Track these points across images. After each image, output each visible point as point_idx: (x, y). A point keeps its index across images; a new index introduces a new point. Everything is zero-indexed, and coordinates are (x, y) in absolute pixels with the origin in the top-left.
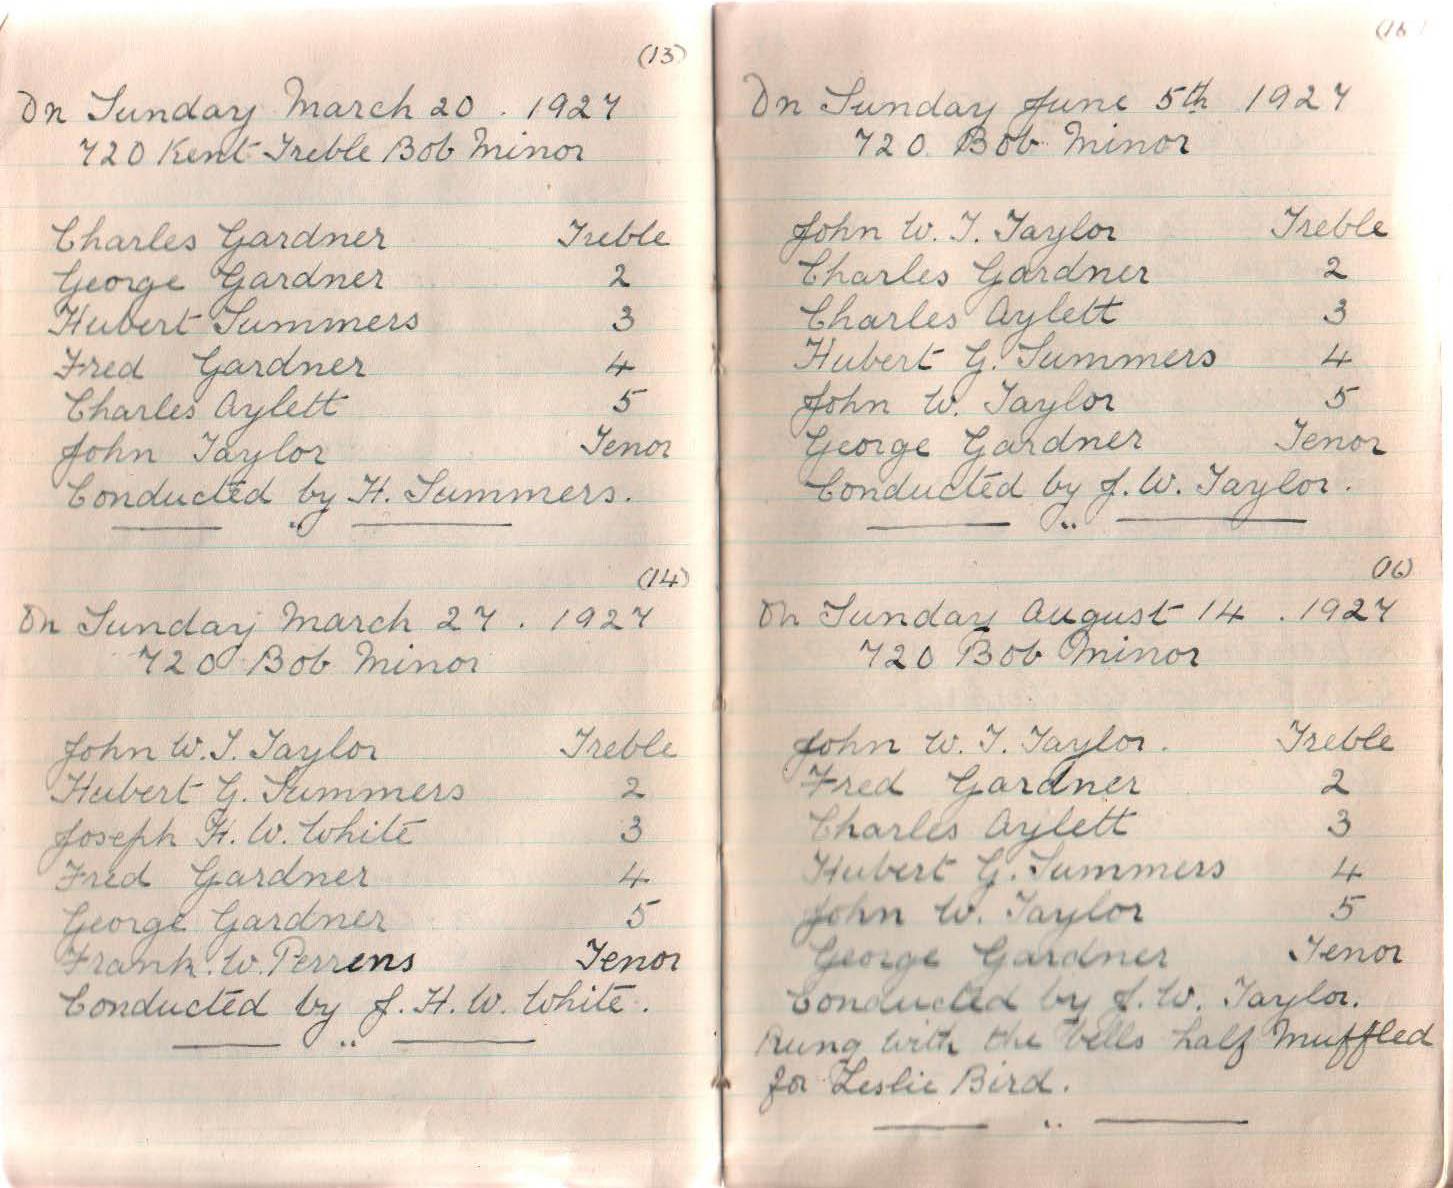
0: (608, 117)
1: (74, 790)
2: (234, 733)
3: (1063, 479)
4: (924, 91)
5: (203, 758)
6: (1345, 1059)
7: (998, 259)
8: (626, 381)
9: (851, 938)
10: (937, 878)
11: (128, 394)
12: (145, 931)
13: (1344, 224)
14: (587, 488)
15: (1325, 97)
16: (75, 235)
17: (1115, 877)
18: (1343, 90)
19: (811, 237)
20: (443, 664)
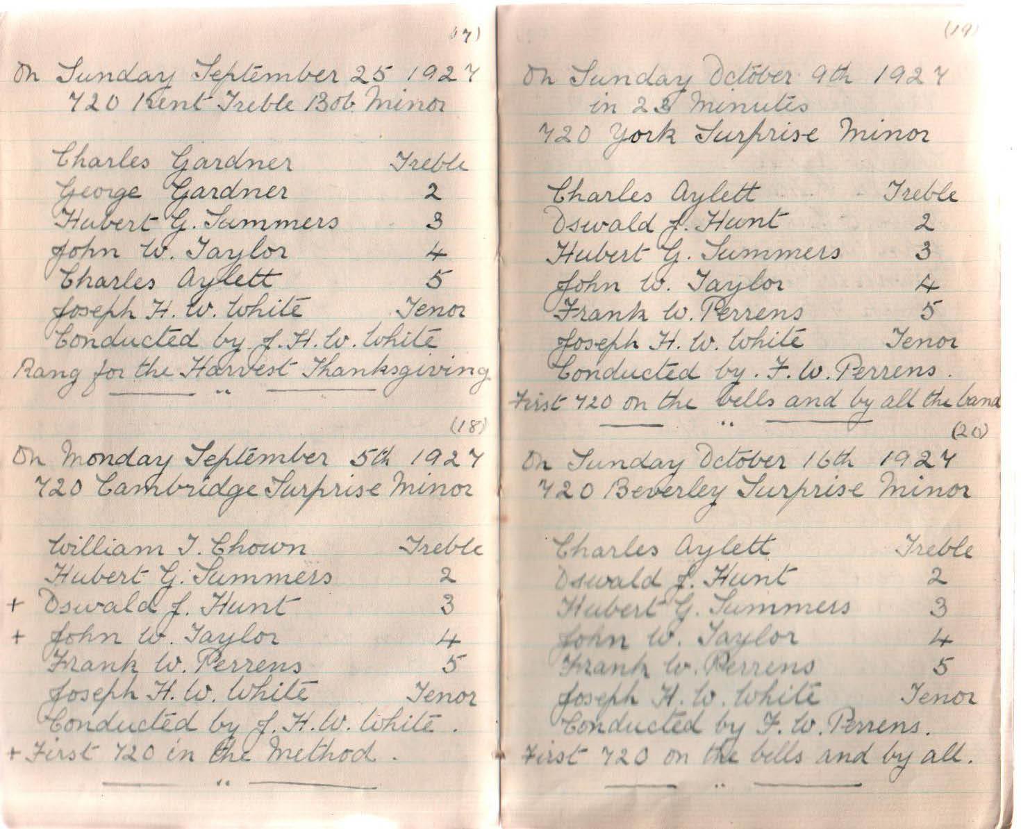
4: (640, 65)
7: (567, 183)
9: (590, 653)
12: (228, 495)
14: (305, 487)
15: (929, 76)
16: (71, 157)
17: (773, 613)
18: (942, 71)
19: (67, 313)
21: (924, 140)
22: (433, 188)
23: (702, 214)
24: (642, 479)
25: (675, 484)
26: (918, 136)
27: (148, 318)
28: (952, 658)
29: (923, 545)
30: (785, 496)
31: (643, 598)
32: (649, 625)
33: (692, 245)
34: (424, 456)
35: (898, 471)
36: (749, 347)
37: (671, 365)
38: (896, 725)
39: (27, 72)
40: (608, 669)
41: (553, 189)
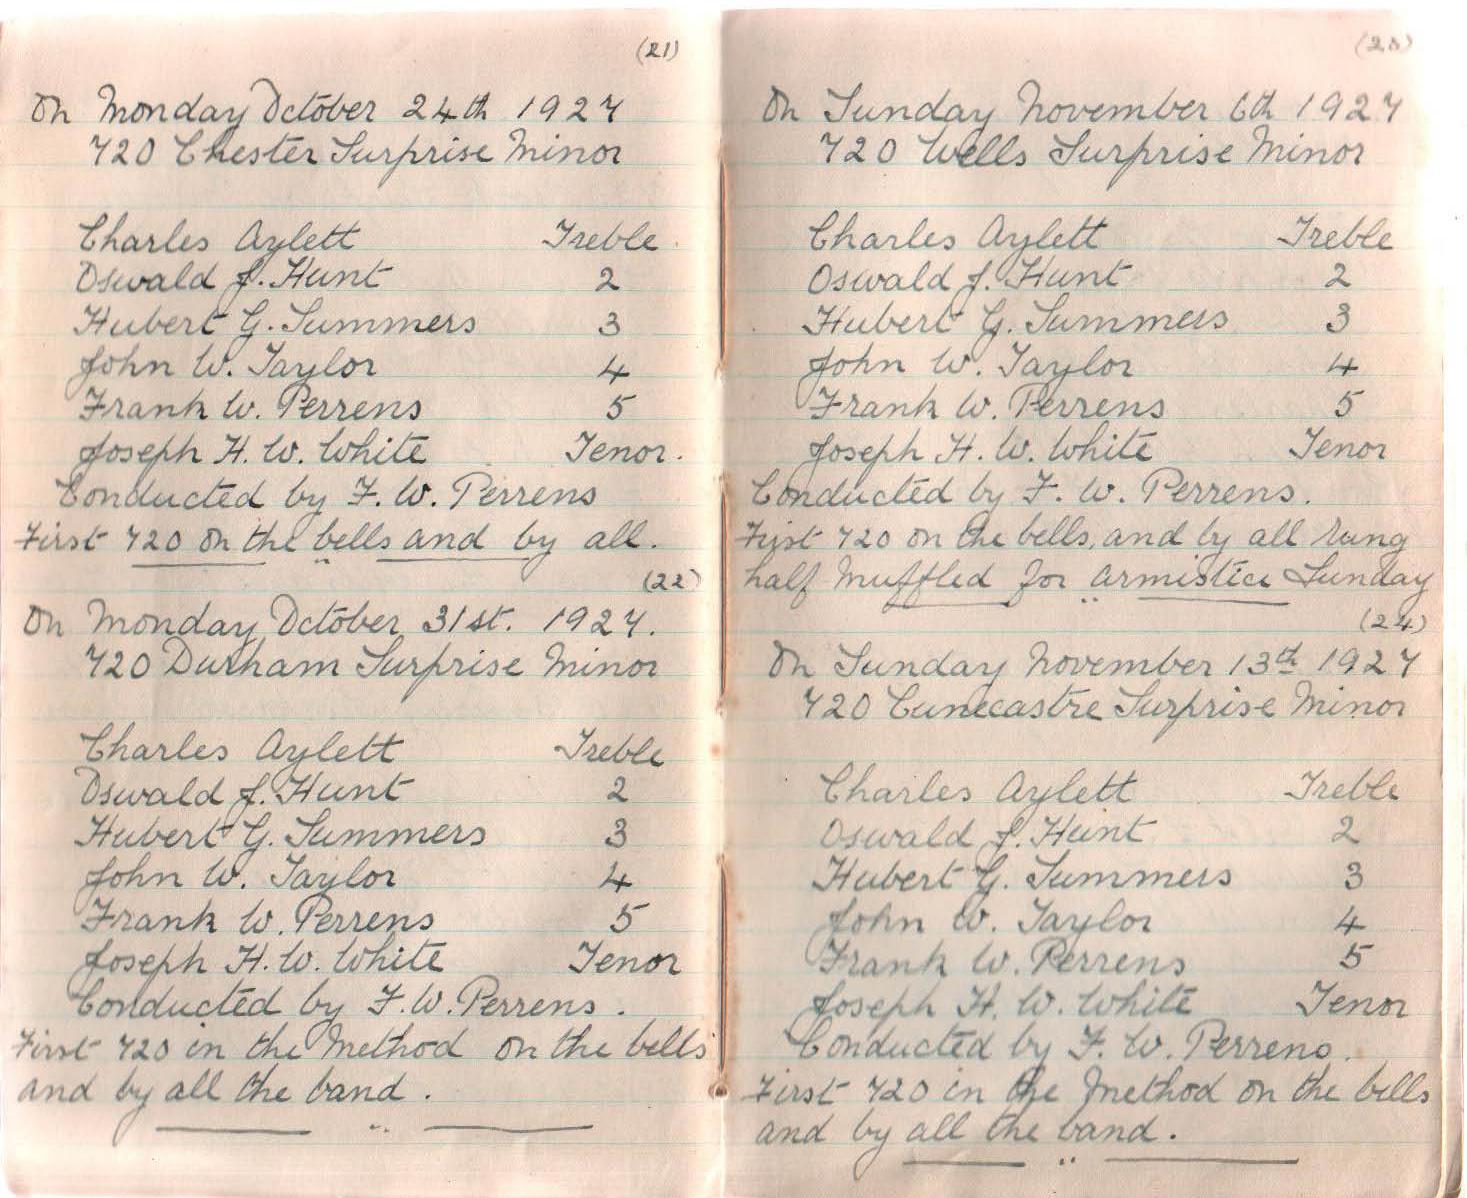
1: (1048, 834)
2: (587, 733)
3: (306, 489)
6: (291, 880)
10: (390, 798)
13: (615, 237)
20: (625, 665)
22: (1340, 269)
23: (278, 268)
24: (937, 691)
25: (992, 698)
28: (1370, 947)
29: (1329, 783)
30: (414, 674)
31: (201, 819)
32: (203, 858)
35: (568, 638)
36: (348, 458)
37: (226, 486)
38: (1292, 1049)
39: (50, 107)
40: (884, 968)
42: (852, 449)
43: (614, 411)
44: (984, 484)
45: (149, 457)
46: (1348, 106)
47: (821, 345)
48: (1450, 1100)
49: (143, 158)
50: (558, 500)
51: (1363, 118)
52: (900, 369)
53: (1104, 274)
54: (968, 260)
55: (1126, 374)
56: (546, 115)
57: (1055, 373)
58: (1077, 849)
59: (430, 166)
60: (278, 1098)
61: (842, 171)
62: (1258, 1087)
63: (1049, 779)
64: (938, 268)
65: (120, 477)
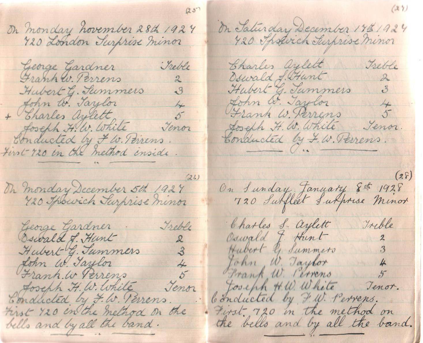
0: (180, 192)
4: (268, 24)
5: (63, 278)
8: (184, 269)
11: (44, 110)
21: (179, 44)
26: (176, 42)
27: (368, 289)
33: (288, 86)
34: (171, 28)
41: (231, 64)
42: (37, 128)
43: (385, 115)
44: (86, 137)
45: (44, 130)
46: (179, 29)
47: (234, 96)
48: (417, 315)
49: (39, 44)
50: (367, 141)
51: (141, 32)
52: (49, 105)
53: (316, 76)
54: (277, 73)
55: (327, 105)
56: (173, 31)
57: (94, 105)
58: (96, 243)
59: (125, 46)
60: (93, 314)
61: (241, 46)
62: (157, 310)
63: (308, 221)
64: (269, 74)
65: (34, 136)
